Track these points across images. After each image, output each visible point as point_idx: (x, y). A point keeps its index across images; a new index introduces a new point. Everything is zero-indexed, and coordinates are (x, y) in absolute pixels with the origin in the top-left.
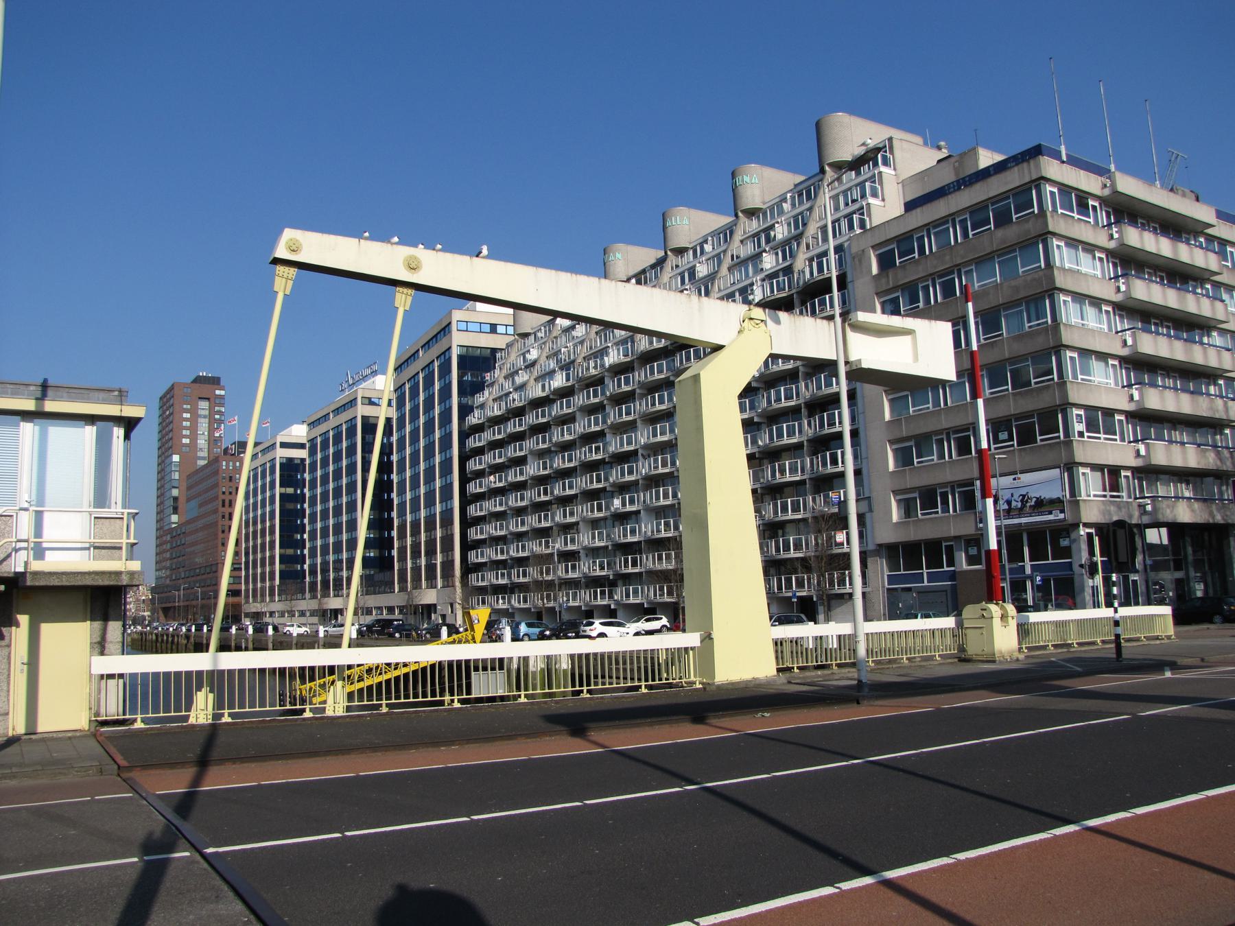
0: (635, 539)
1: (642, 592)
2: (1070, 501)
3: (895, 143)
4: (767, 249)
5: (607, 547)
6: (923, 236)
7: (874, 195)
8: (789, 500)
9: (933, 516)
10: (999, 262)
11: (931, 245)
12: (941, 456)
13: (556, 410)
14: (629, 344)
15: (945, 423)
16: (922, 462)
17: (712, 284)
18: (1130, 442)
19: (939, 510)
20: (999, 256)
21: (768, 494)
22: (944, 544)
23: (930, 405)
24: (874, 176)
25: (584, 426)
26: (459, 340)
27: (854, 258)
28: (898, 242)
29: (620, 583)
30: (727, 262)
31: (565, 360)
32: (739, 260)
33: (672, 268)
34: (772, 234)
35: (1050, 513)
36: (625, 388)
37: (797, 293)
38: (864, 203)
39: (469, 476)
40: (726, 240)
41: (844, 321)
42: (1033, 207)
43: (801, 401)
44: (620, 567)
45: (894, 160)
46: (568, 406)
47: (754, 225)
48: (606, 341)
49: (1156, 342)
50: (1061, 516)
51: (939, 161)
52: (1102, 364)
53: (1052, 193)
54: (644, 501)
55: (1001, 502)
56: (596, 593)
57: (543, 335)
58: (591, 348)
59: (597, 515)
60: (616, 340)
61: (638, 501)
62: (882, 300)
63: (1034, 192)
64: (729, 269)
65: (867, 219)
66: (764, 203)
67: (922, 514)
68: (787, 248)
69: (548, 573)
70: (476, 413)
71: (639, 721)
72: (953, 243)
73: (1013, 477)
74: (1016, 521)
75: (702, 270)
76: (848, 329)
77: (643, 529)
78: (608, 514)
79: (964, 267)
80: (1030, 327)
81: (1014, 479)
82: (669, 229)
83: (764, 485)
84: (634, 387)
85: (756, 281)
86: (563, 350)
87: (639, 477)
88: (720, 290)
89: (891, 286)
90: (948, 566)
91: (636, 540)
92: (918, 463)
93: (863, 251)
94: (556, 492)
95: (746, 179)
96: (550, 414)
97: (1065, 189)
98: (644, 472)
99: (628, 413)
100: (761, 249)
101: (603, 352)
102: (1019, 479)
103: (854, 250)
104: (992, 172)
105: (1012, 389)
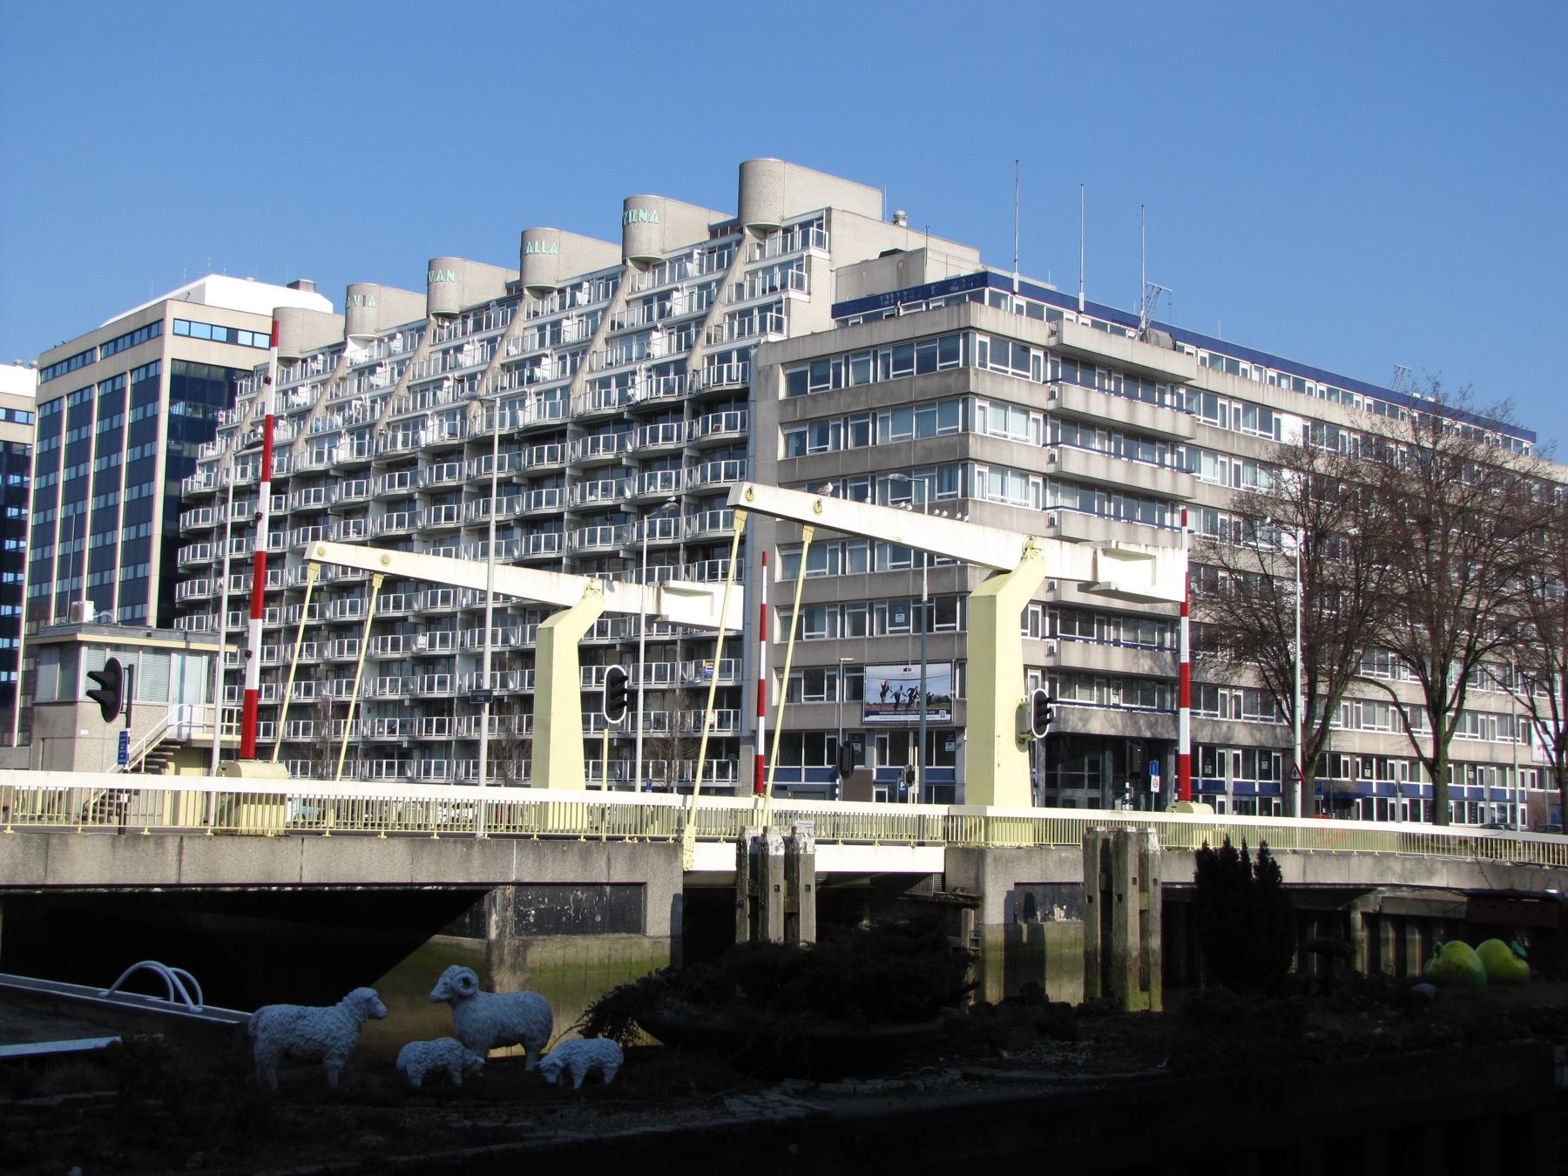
0: (445, 695)
1: (448, 769)
2: (958, 702)
3: (834, 215)
4: (659, 326)
5: (401, 702)
6: (841, 363)
7: (820, 242)
8: (654, 664)
9: (818, 702)
10: (917, 415)
11: (849, 378)
12: (833, 633)
13: (338, 494)
14: (458, 417)
15: (840, 595)
16: (812, 637)
17: (582, 359)
18: (1044, 637)
19: (825, 696)
20: (918, 408)
21: (629, 653)
22: (826, 737)
23: (827, 570)
24: (801, 259)
25: (382, 524)
26: (175, 349)
27: (759, 373)
28: (812, 363)
29: (416, 753)
30: (605, 330)
31: (357, 420)
32: (621, 331)
33: (529, 314)
34: (668, 305)
35: (937, 712)
36: (447, 482)
37: (688, 400)
38: (784, 297)
39: (180, 571)
40: (606, 295)
41: (661, 585)
42: (958, 359)
43: (681, 540)
44: (420, 731)
45: (830, 239)
46: (359, 492)
47: (646, 283)
48: (423, 405)
49: (1087, 523)
50: (948, 717)
51: (883, 254)
52: (1211, 460)
53: (983, 344)
54: (462, 644)
55: (889, 694)
56: (379, 765)
57: (320, 367)
58: (399, 411)
59: (390, 654)
60: (438, 409)
61: (453, 641)
62: (786, 432)
63: (961, 341)
64: (607, 340)
65: (806, 275)
66: (664, 252)
67: (806, 699)
68: (685, 330)
69: (306, 730)
70: (201, 475)
71: (469, 888)
72: (871, 381)
73: (904, 667)
74: (902, 718)
75: (571, 331)
76: (662, 591)
77: (458, 682)
78: (408, 655)
79: (881, 412)
80: (940, 497)
81: (905, 670)
82: (529, 258)
83: (624, 642)
84: (460, 483)
85: (640, 369)
86: (354, 402)
87: (458, 609)
88: (591, 370)
89: (798, 418)
90: (828, 764)
91: (445, 696)
92: (807, 637)
93: (771, 366)
94: (329, 614)
95: (643, 215)
96: (328, 498)
97: (999, 340)
98: (464, 602)
99: (449, 517)
100: (651, 325)
101: (417, 423)
102: (910, 670)
103: (761, 363)
104: (933, 292)
105: (915, 566)
